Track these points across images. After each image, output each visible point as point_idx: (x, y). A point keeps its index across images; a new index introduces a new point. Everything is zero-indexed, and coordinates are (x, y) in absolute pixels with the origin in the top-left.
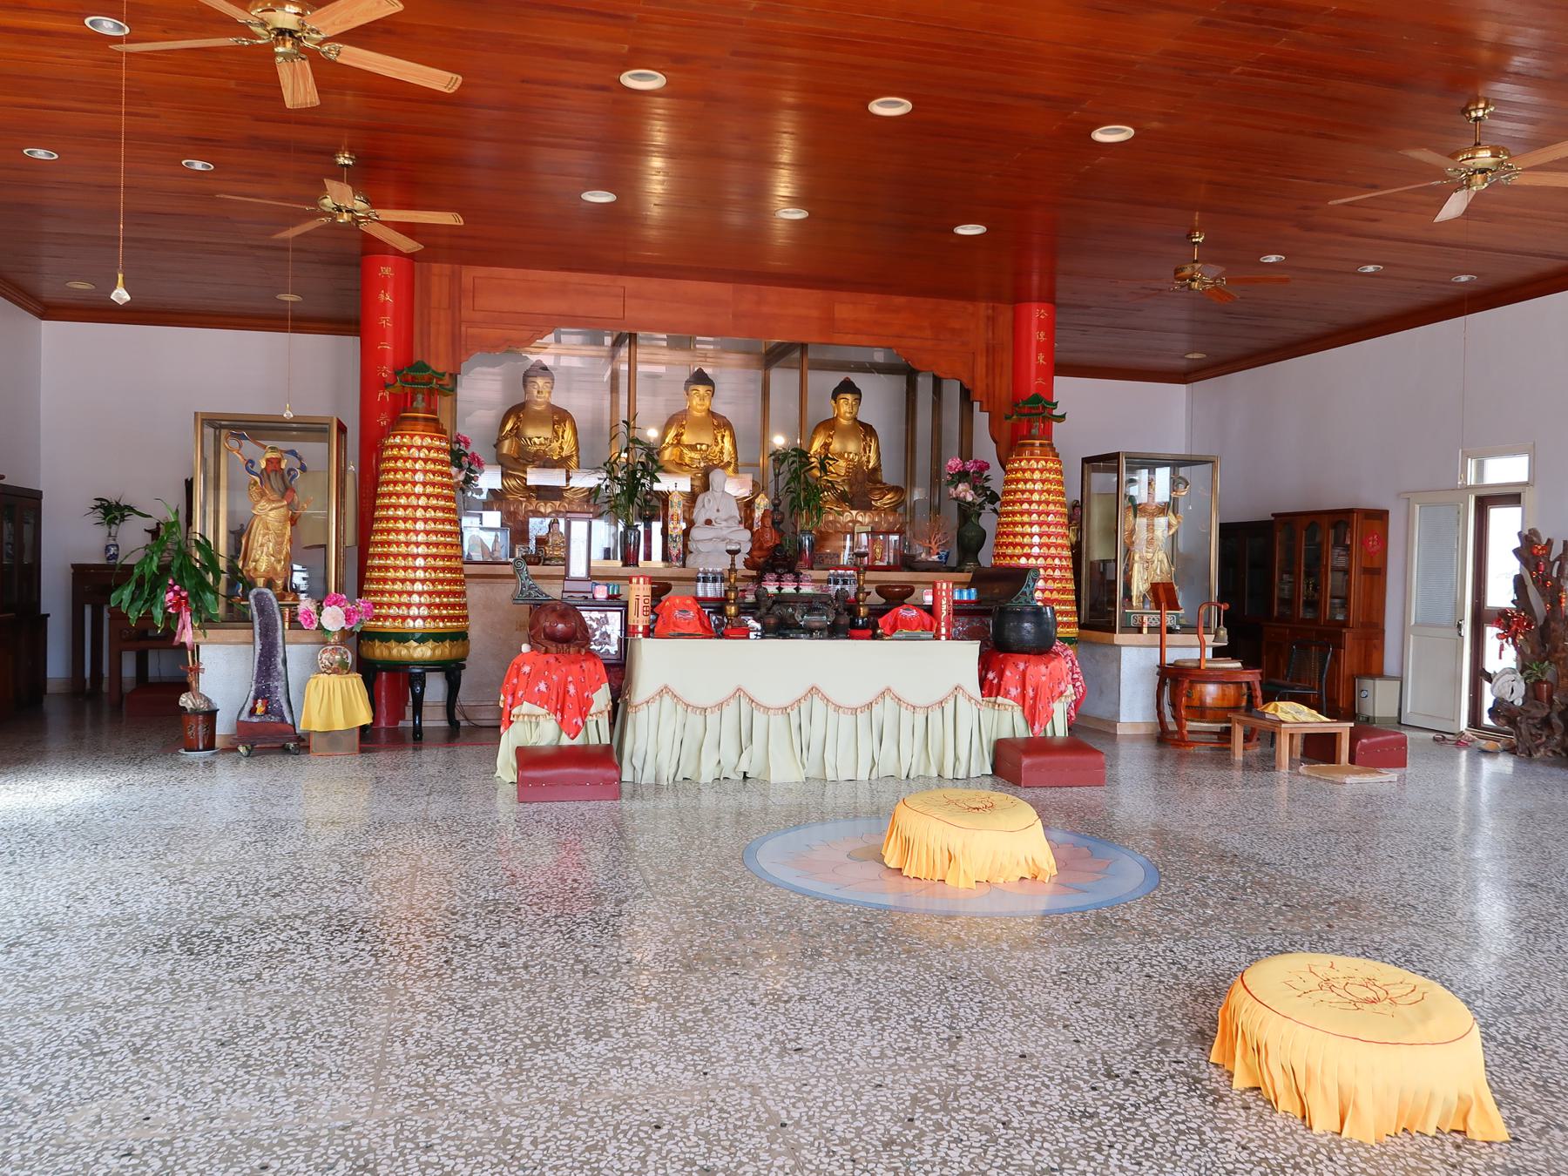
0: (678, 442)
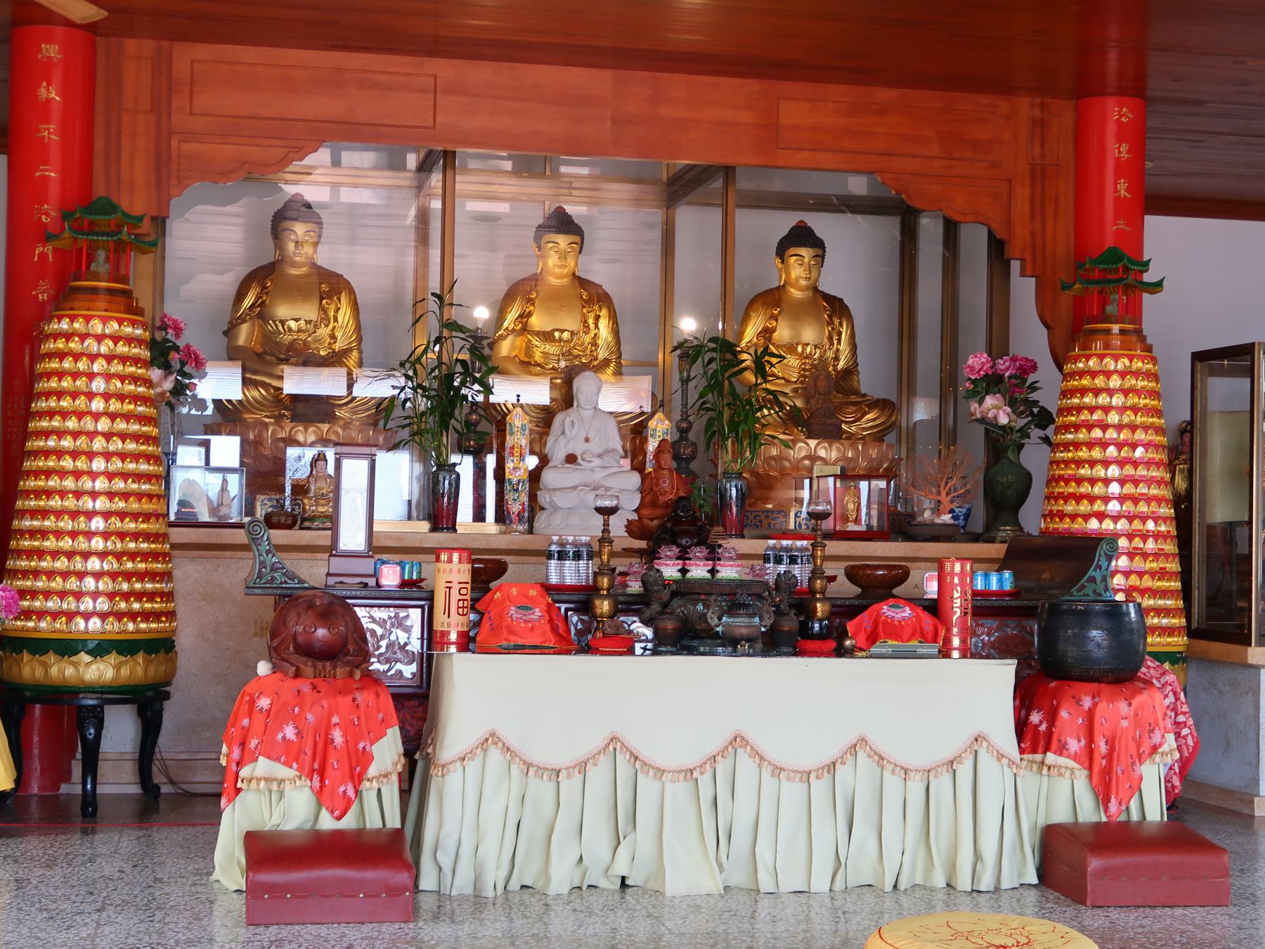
0: (524, 328)
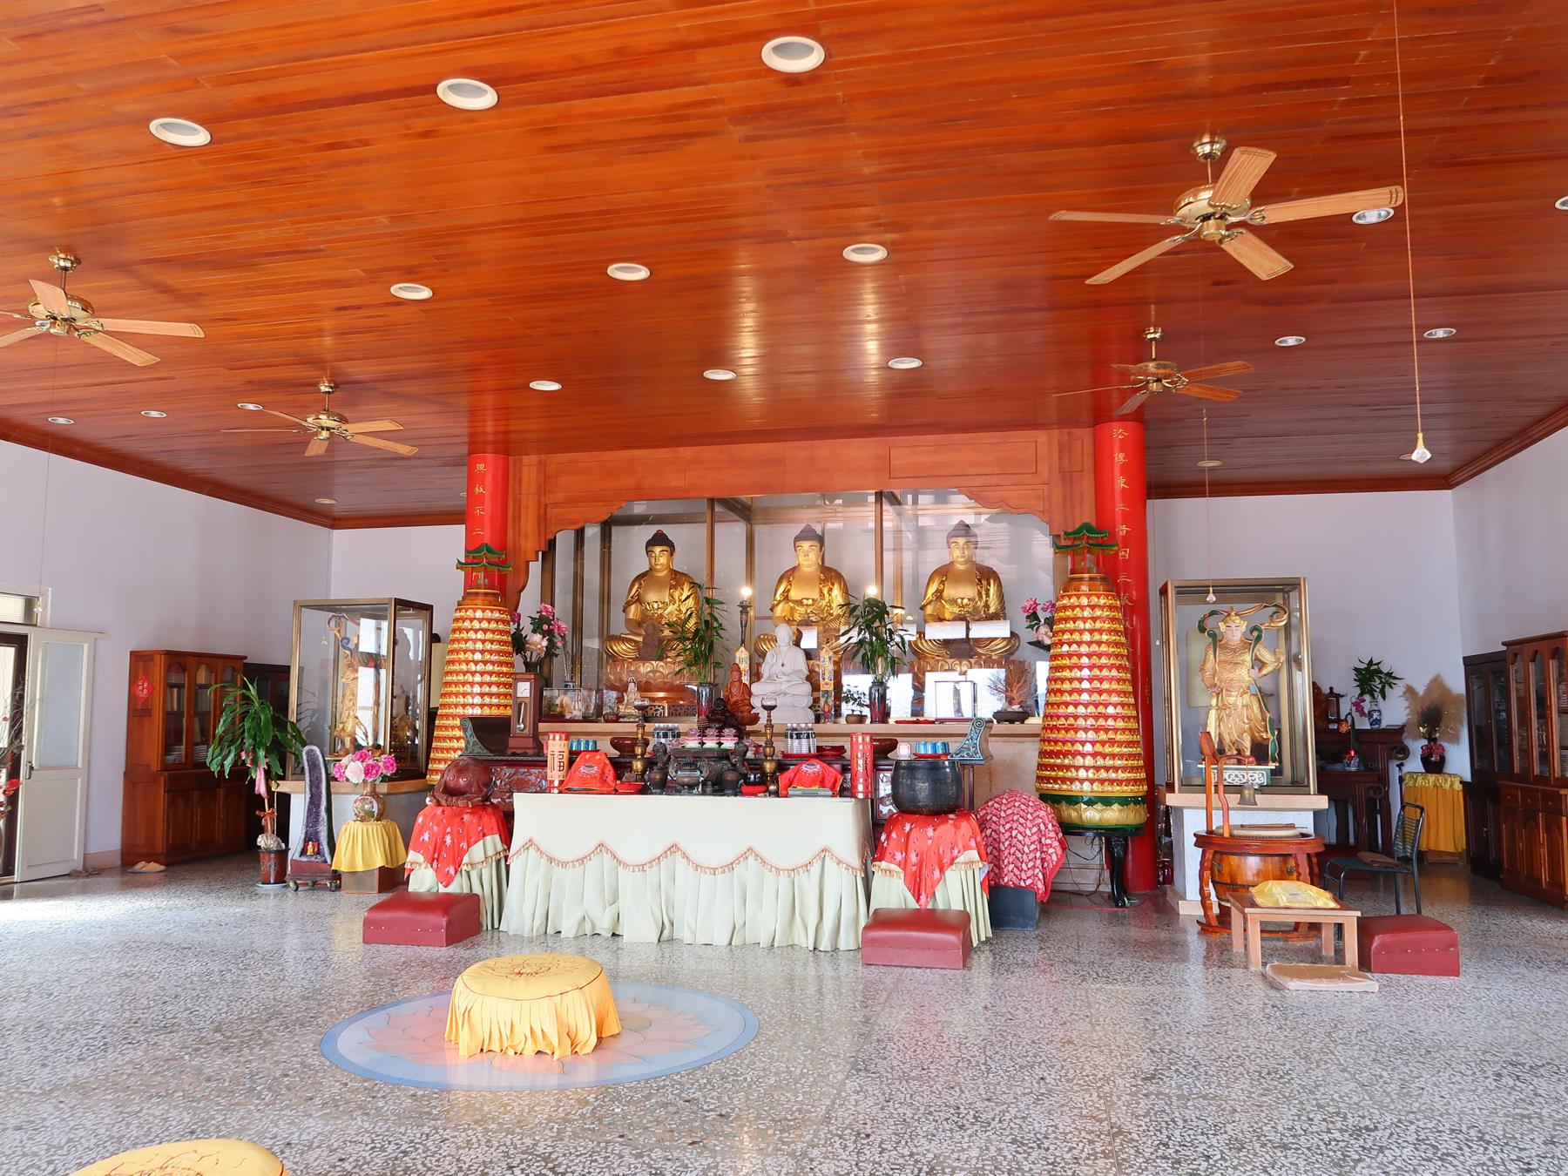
0: (786, 598)
